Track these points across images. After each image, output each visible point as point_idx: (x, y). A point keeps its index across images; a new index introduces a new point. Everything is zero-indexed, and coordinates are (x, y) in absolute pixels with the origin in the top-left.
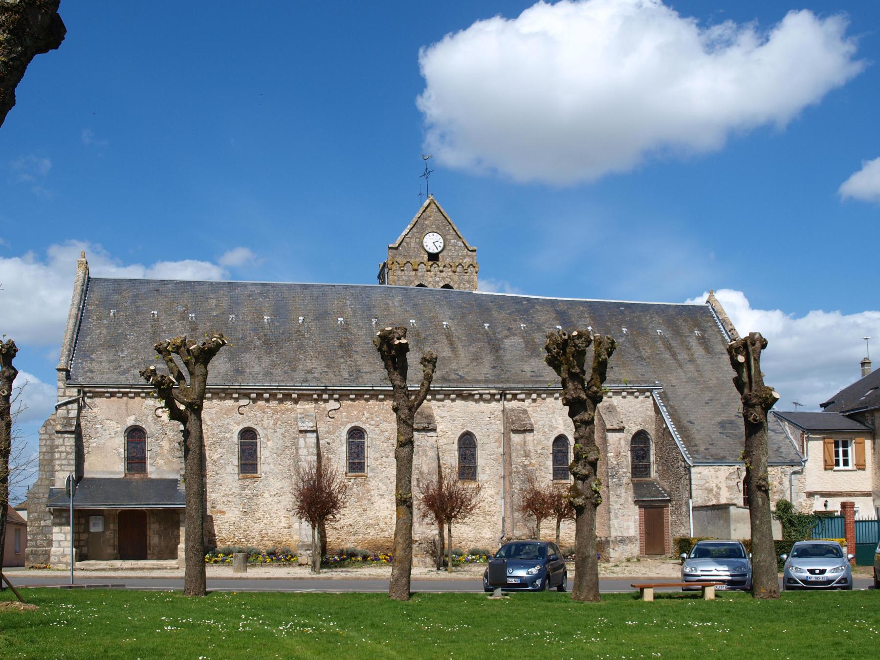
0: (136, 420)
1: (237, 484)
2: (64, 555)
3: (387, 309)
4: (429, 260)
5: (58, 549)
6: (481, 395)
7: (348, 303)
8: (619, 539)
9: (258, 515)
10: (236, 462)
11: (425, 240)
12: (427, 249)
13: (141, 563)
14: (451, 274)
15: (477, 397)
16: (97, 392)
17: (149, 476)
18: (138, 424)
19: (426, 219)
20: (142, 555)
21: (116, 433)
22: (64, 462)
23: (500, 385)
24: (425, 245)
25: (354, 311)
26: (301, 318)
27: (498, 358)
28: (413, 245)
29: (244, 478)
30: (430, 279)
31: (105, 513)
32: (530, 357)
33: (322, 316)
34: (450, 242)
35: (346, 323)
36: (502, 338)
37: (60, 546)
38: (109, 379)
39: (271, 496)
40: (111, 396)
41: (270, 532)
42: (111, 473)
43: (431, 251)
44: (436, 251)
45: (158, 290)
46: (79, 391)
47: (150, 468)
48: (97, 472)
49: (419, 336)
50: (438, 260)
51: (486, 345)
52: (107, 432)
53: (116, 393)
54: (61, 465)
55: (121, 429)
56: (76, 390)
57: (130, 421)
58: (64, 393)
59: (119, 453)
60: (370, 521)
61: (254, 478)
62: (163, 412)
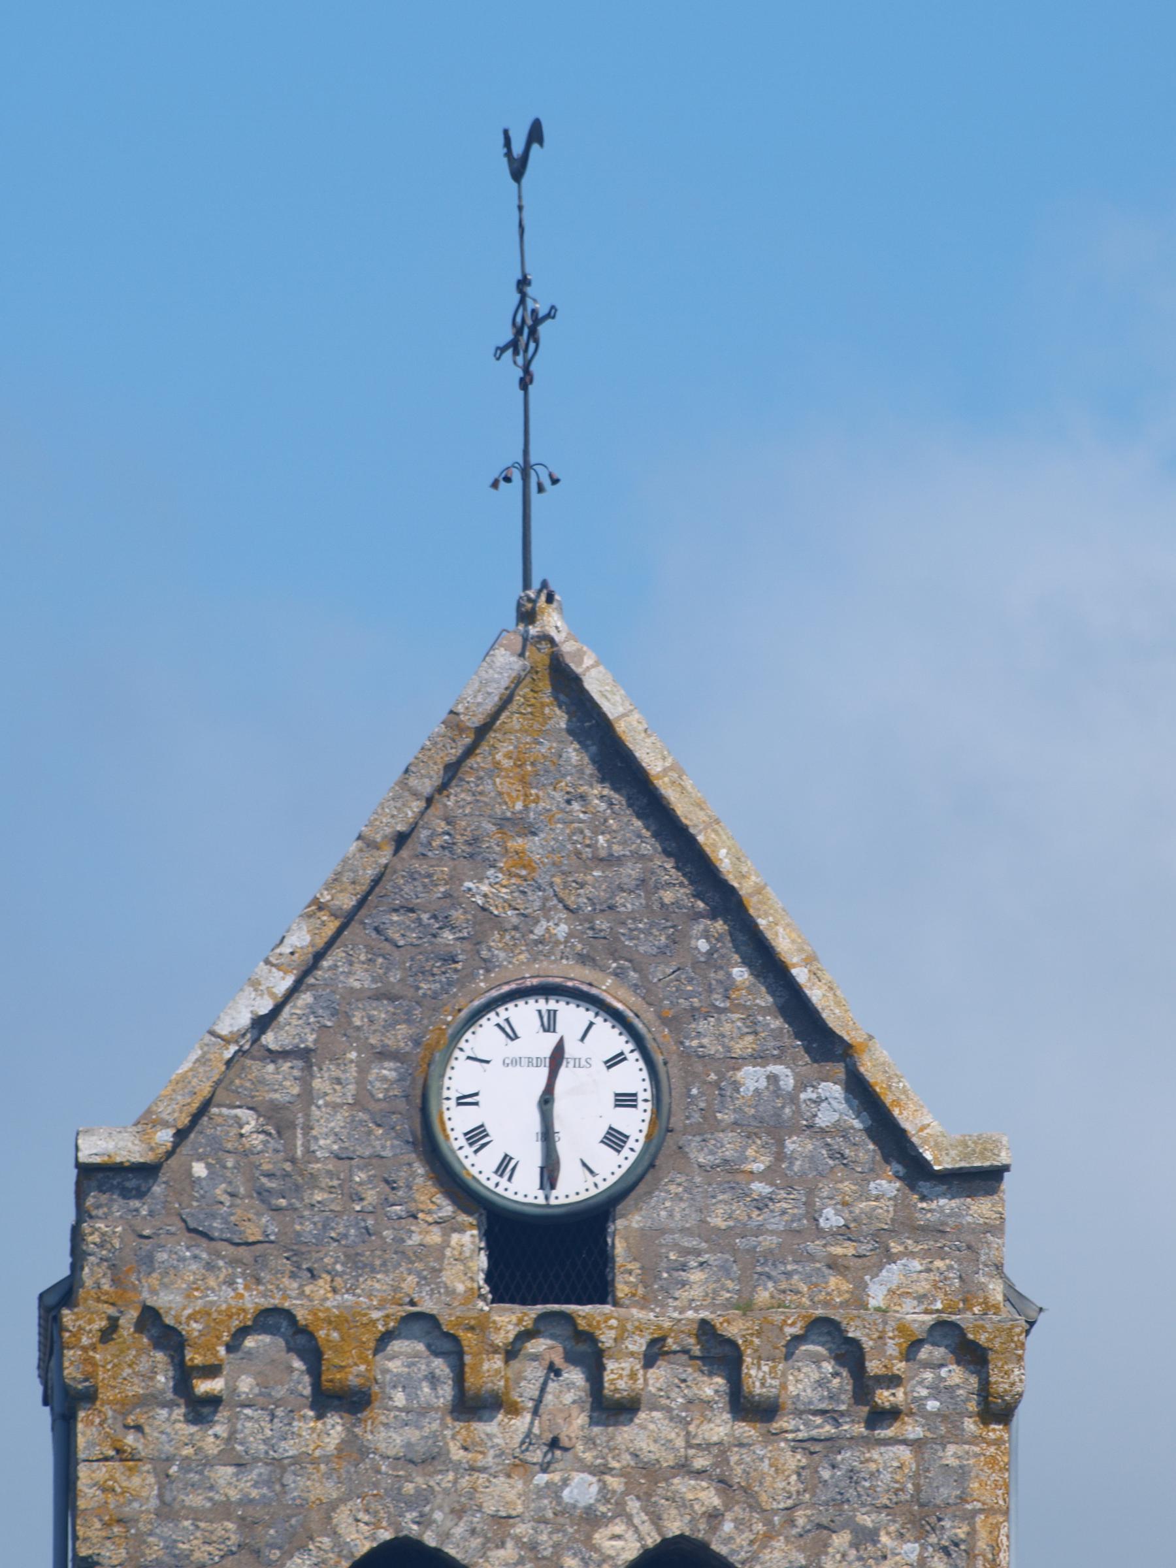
4: (505, 1284)
28: (327, 1131)
44: (574, 1188)
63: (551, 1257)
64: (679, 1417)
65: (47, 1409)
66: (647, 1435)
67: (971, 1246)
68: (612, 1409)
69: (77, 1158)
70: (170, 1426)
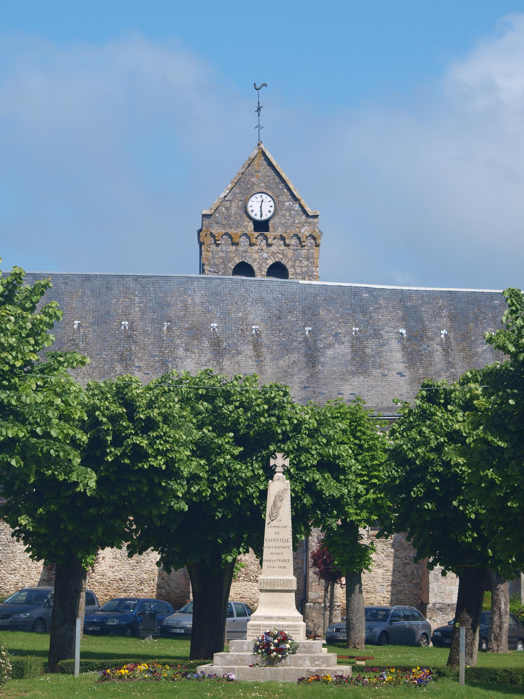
3: (186, 307)
4: (256, 229)
7: (137, 299)
8: (438, 606)
9: (13, 565)
11: (250, 203)
12: (252, 215)
14: (283, 247)
19: (252, 176)
24: (250, 209)
25: (143, 311)
26: (76, 322)
27: (313, 376)
28: (233, 210)
30: (255, 256)
32: (353, 374)
33: (103, 319)
34: (283, 205)
35: (131, 328)
36: (324, 348)
43: (258, 218)
44: (264, 218)
49: (219, 346)
50: (267, 230)
51: (302, 358)
60: (145, 576)
63: (262, 226)
66: (273, 249)
67: (314, 225)
70: (213, 247)
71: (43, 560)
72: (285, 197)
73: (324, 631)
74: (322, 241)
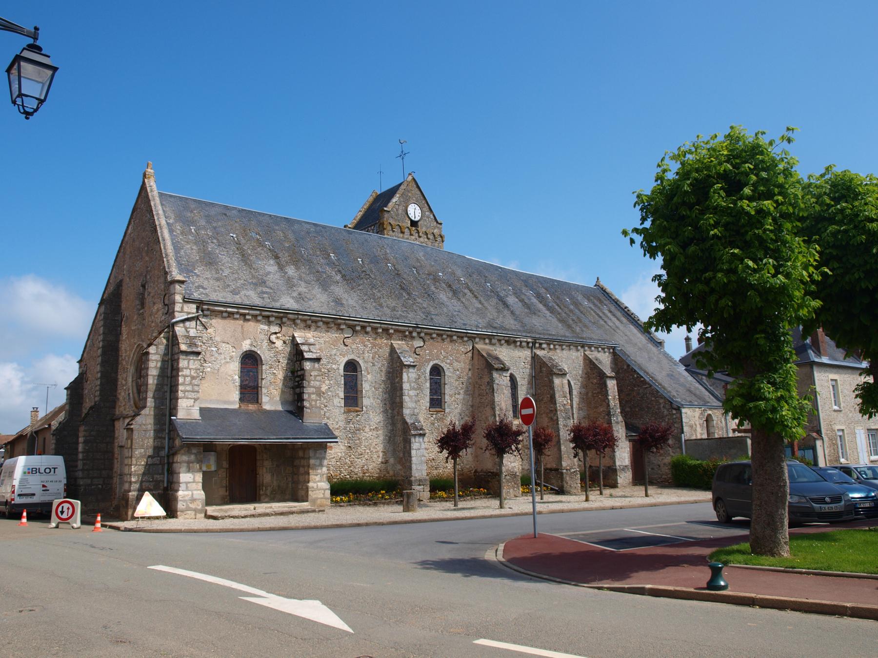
0: (251, 345)
1: (342, 417)
2: (193, 500)
4: (412, 225)
5: (186, 493)
6: (521, 342)
9: (360, 450)
10: (342, 395)
13: (249, 508)
15: (518, 344)
16: (214, 311)
17: (264, 407)
18: (253, 349)
20: (252, 497)
21: (231, 357)
22: (189, 388)
23: (533, 335)
28: (400, 211)
29: (349, 411)
31: (218, 449)
37: (187, 489)
38: (223, 297)
39: (371, 430)
40: (229, 317)
41: (370, 467)
42: (225, 402)
44: (416, 219)
45: (225, 215)
46: (198, 308)
47: (265, 399)
48: (211, 401)
52: (223, 356)
53: (233, 313)
54: (184, 391)
55: (237, 355)
56: (194, 306)
57: (246, 346)
58: (182, 308)
59: (234, 380)
61: (357, 411)
62: (277, 338)
63: (414, 224)
64: (423, 239)
65: (674, 327)
66: (421, 239)
67: (440, 229)
68: (420, 237)
69: (165, 518)
70: (391, 232)
71: (659, 254)
72: (426, 209)
73: (585, 464)
74: (445, 239)
